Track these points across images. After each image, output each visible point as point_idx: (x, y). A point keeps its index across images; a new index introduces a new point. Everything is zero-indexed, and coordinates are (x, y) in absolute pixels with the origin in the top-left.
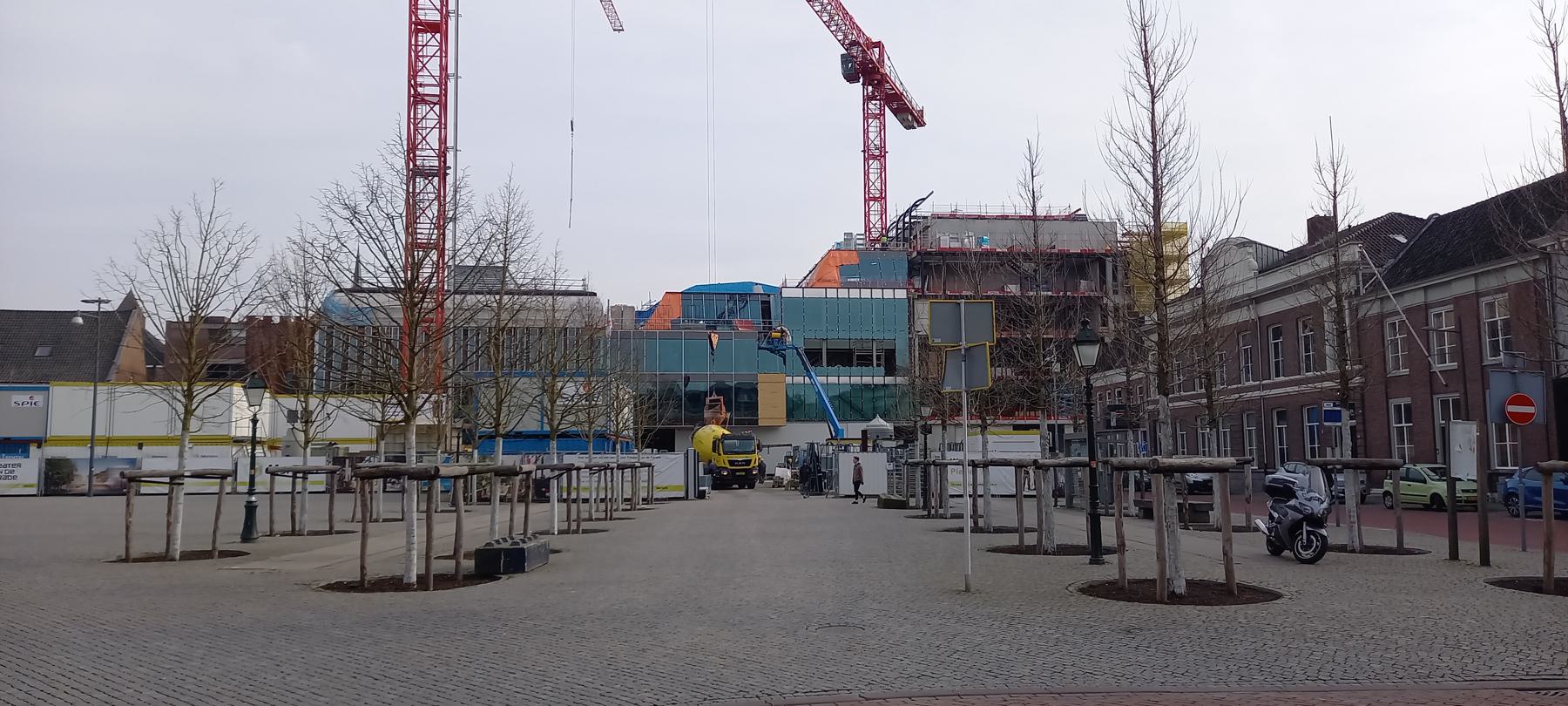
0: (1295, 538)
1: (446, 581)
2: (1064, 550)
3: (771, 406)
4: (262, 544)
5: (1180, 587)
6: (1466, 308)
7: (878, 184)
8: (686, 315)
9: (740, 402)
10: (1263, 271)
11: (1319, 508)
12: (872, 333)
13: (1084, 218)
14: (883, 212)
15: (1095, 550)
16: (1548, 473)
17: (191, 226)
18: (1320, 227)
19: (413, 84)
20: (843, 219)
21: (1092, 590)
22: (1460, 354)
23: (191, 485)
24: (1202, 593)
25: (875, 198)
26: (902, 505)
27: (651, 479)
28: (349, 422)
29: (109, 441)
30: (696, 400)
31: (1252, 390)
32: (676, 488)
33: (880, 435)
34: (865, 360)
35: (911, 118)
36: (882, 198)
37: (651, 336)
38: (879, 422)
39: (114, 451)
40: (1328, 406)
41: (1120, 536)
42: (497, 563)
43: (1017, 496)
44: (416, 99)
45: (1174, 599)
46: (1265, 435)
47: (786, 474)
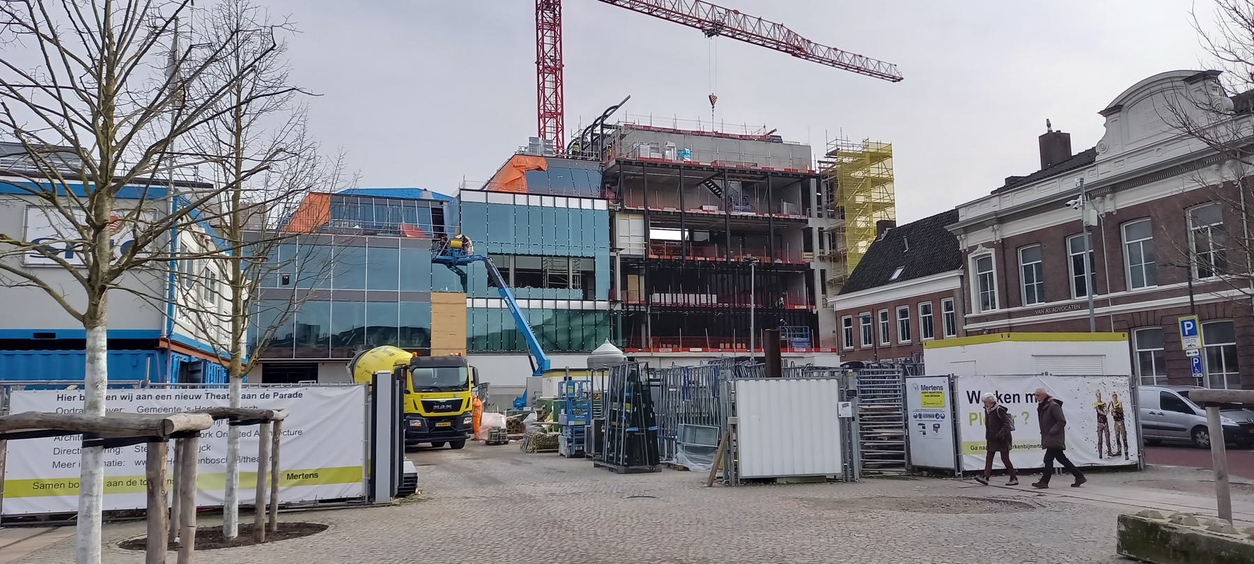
7: (553, 100)
13: (778, 140)
14: (559, 128)
20: (518, 130)
25: (551, 113)
32: (341, 475)
34: (559, 281)
36: (557, 114)
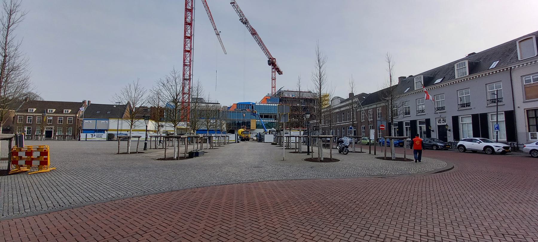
0: (343, 150)
1: (182, 158)
2: (303, 152)
3: (253, 125)
4: (148, 150)
5: (322, 159)
6: (375, 110)
8: (237, 108)
9: (247, 125)
10: (341, 103)
11: (348, 145)
12: (272, 112)
14: (275, 90)
15: (308, 153)
16: (386, 138)
17: (133, 88)
18: (351, 95)
19: (184, 62)
20: (267, 91)
21: (307, 160)
22: (373, 118)
23: (132, 139)
24: (326, 160)
25: (274, 87)
26: (276, 144)
27: (228, 139)
28: (169, 127)
29: (121, 130)
30: (239, 124)
31: (338, 124)
33: (273, 131)
34: (271, 117)
35: (280, 72)
37: (230, 112)
38: (273, 129)
39: (122, 132)
40: (351, 127)
41: (312, 150)
42: (193, 155)
43: (296, 143)
44: (185, 65)
45: (321, 161)
46: (341, 132)
47: (255, 138)
